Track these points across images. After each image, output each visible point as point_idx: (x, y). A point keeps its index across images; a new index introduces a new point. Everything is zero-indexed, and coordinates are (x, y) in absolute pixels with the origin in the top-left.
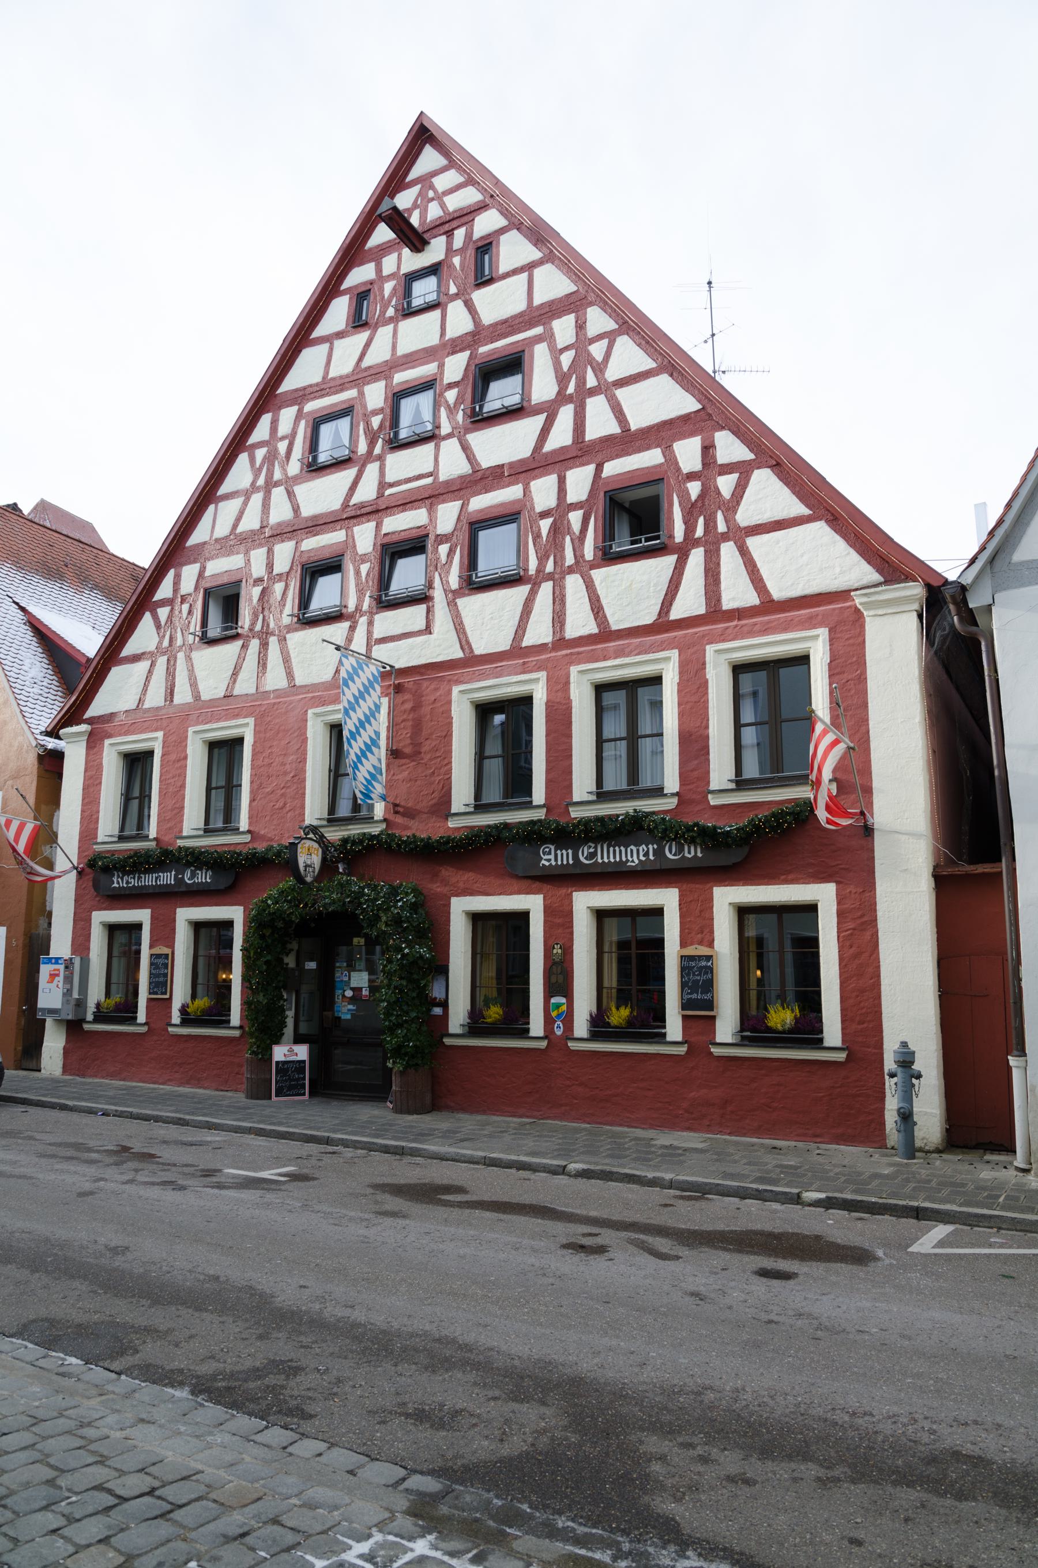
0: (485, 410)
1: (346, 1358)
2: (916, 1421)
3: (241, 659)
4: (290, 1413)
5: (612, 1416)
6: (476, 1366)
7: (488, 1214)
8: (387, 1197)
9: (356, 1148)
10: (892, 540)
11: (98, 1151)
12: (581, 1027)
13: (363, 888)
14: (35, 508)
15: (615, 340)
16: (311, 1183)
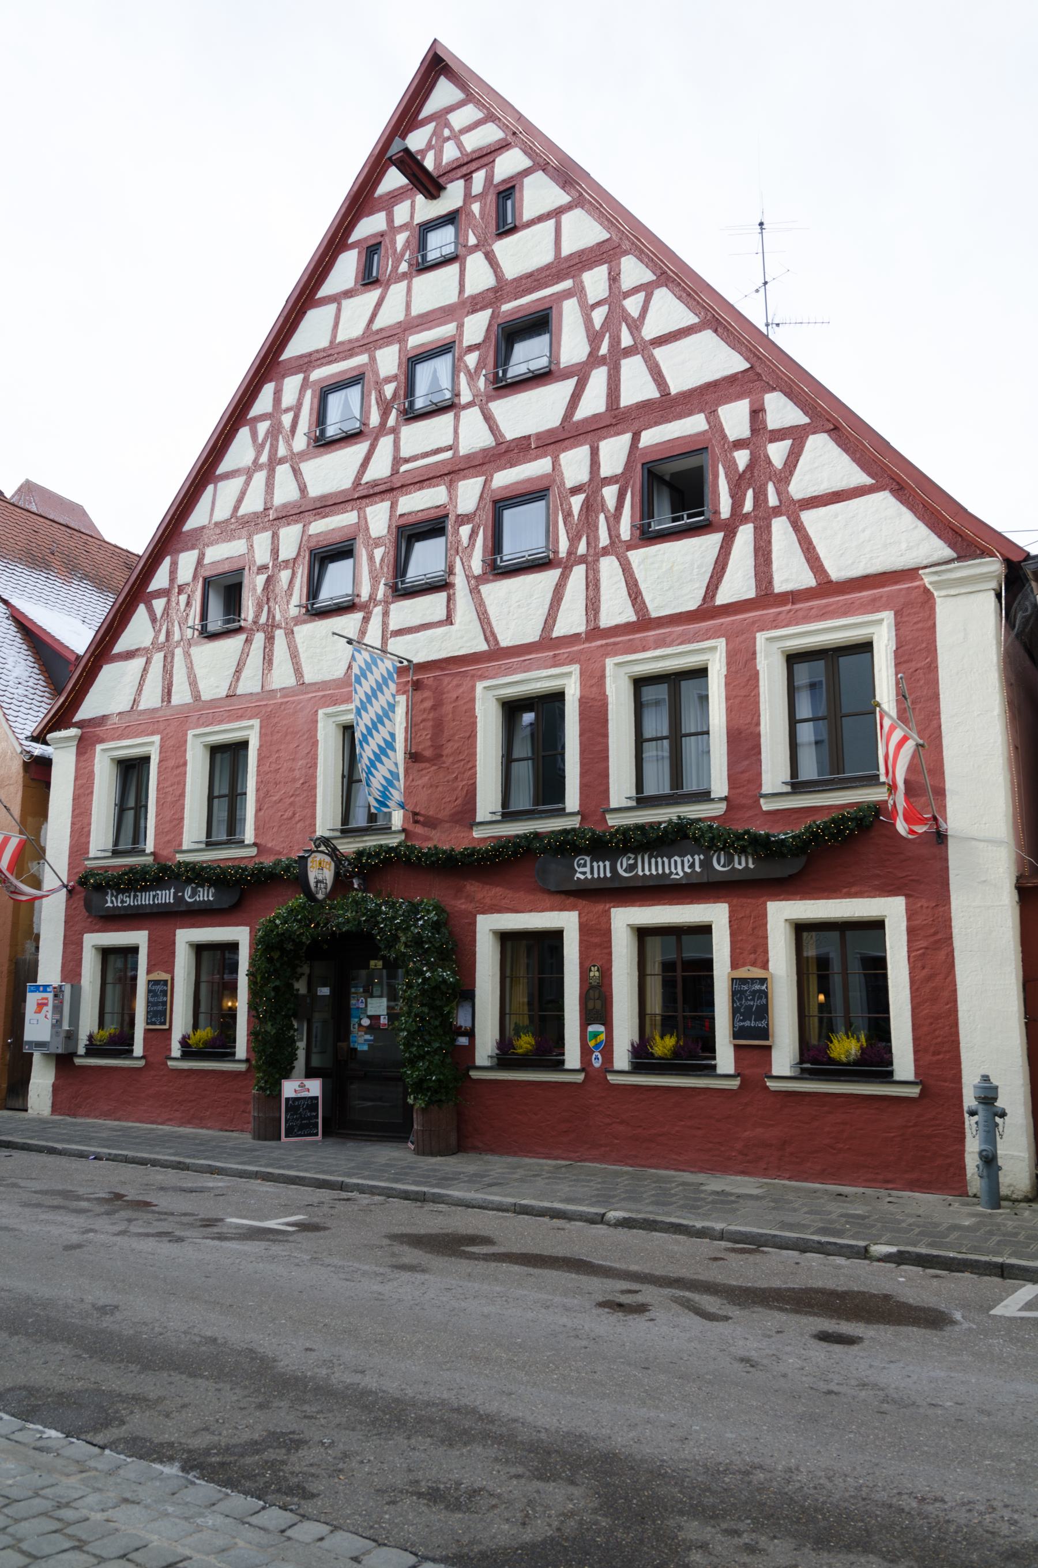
0: (510, 374)
1: (353, 1430)
2: (994, 1509)
3: (244, 655)
4: (290, 1491)
5: (648, 1497)
6: (498, 1439)
7: (516, 1268)
8: (406, 1248)
9: (373, 1194)
10: (965, 510)
11: (88, 1200)
12: (622, 1059)
13: (380, 906)
14: (19, 490)
15: (652, 293)
16: (322, 1233)
